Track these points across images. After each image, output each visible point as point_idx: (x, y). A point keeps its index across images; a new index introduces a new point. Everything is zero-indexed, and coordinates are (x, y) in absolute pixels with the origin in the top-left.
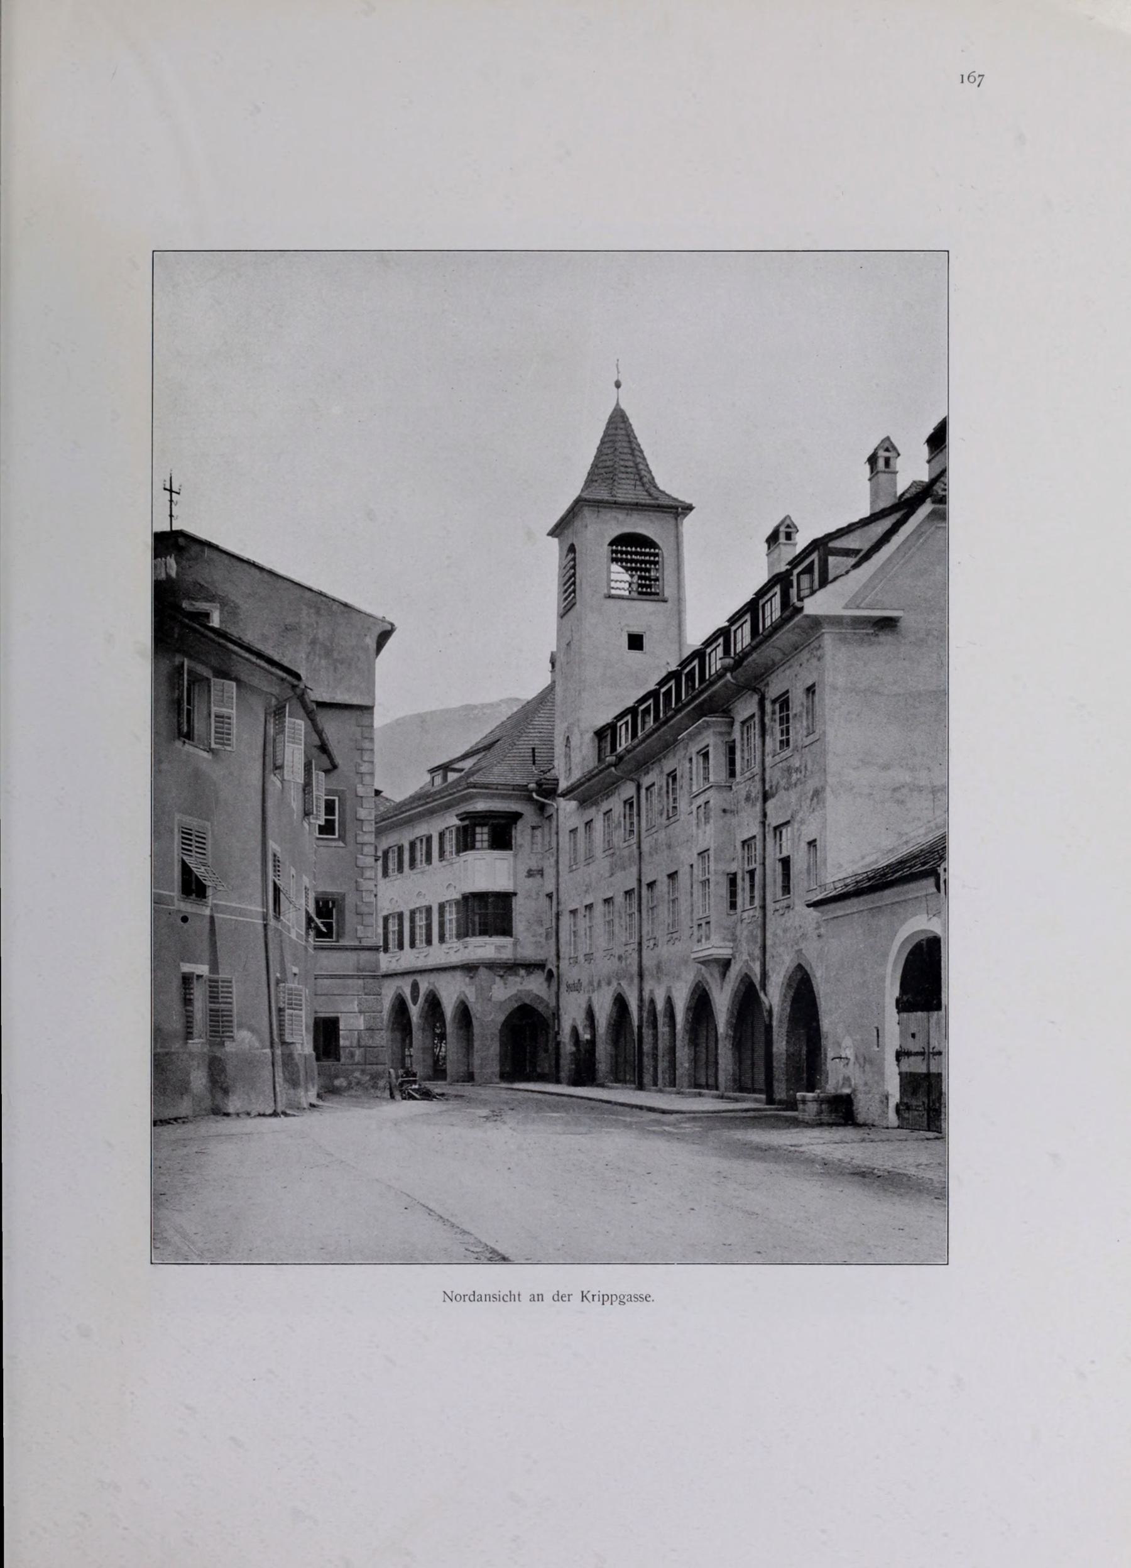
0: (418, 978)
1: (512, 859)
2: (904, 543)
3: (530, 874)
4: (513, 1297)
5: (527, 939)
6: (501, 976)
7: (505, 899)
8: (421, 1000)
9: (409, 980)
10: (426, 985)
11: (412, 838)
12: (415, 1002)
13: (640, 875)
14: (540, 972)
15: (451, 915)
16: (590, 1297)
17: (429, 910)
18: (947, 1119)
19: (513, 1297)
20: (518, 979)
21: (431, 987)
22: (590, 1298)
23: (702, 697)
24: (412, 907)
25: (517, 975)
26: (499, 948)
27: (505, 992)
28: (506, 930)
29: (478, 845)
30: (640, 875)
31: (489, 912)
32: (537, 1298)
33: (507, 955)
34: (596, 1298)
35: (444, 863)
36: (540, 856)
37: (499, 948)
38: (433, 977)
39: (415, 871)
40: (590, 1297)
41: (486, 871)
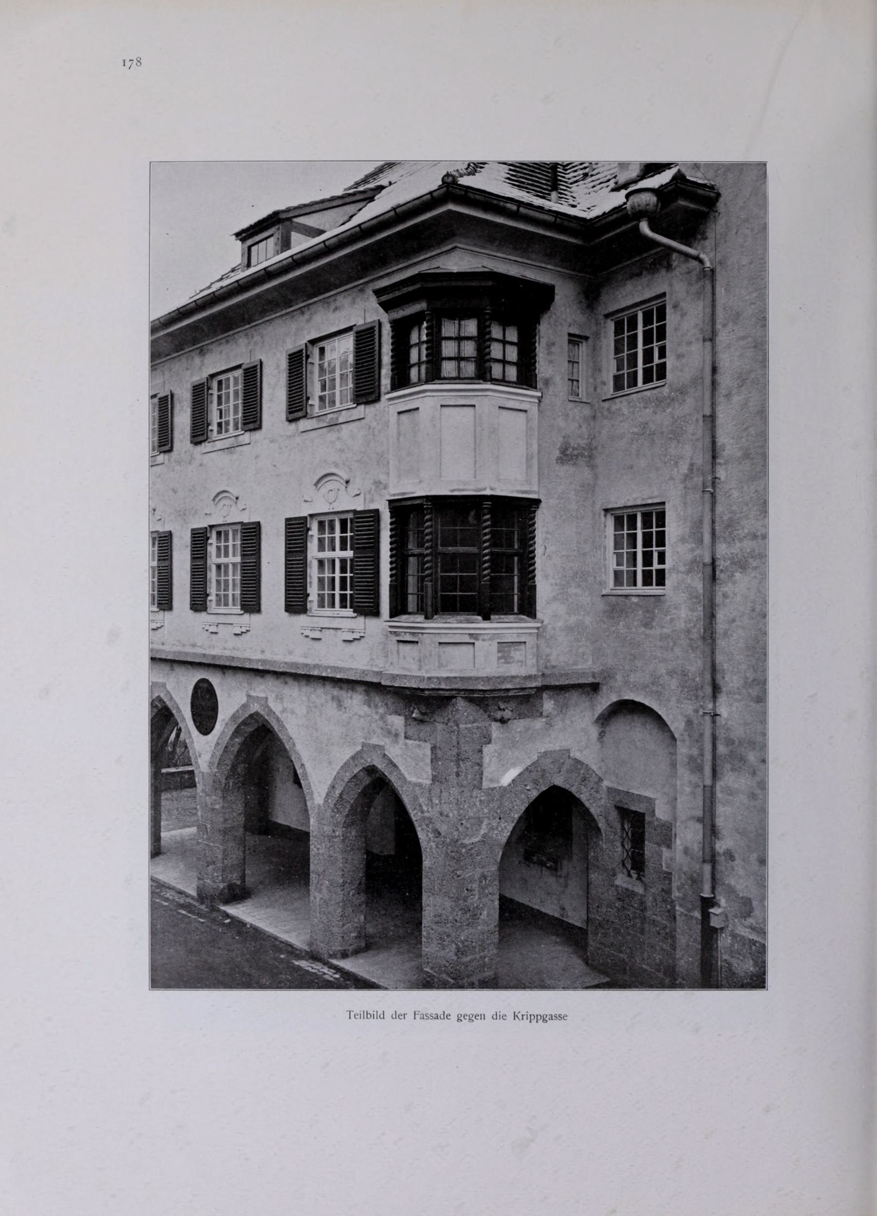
1: (534, 410)
2: (341, 396)
3: (567, 455)
5: (569, 610)
6: (503, 721)
7: (513, 516)
11: (200, 376)
15: (324, 554)
16: (520, 1016)
17: (252, 534)
21: (255, 708)
22: (520, 1017)
24: (201, 523)
26: (505, 648)
27: (510, 763)
29: (448, 368)
31: (465, 555)
33: (522, 667)
34: (525, 1017)
35: (304, 424)
36: (587, 411)
37: (182, 432)
38: (263, 689)
39: (206, 447)
40: (520, 1016)
41: (459, 438)
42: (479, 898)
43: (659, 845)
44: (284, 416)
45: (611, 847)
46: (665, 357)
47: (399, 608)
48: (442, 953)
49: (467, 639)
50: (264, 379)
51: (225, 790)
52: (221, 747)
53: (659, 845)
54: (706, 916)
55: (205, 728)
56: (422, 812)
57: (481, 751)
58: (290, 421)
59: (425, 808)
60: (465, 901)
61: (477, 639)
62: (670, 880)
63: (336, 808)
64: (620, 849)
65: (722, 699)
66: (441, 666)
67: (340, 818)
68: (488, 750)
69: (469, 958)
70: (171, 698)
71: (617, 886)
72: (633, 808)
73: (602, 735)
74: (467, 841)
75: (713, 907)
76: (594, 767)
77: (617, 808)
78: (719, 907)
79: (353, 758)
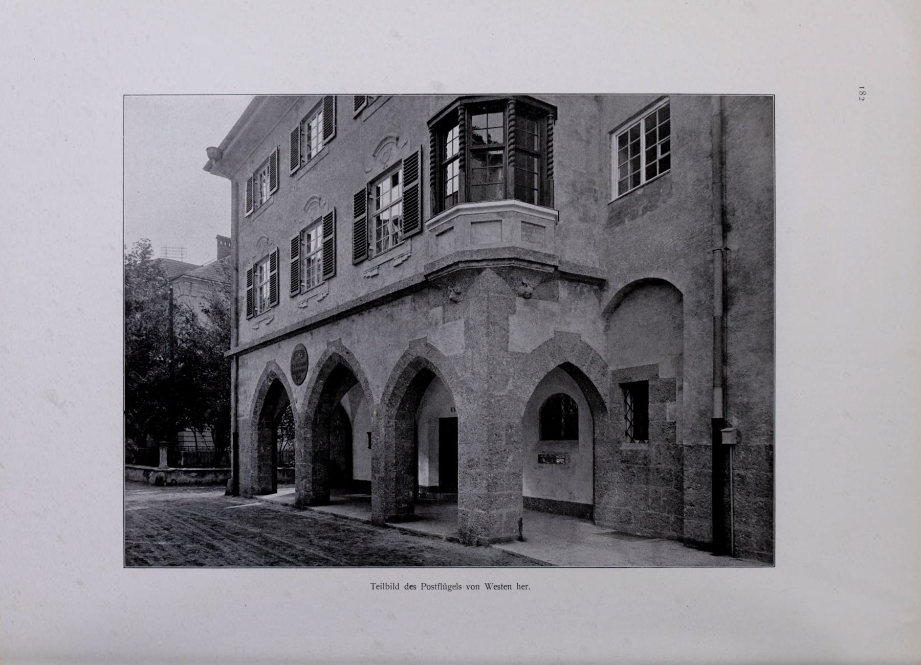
0: (305, 340)
4: (396, 587)
6: (526, 296)
8: (311, 376)
9: (288, 348)
10: (322, 347)
12: (298, 380)
13: (721, 184)
14: (593, 299)
18: (755, 565)
19: (396, 587)
20: (554, 307)
23: (233, 394)
25: (554, 298)
28: (533, 187)
30: (721, 184)
32: (412, 587)
38: (336, 332)
42: (507, 444)
43: (663, 401)
44: (350, 261)
45: (618, 420)
46: (634, 160)
47: (426, 476)
48: (475, 491)
49: (496, 218)
50: (338, 264)
51: (315, 424)
52: (310, 390)
53: (663, 401)
54: (717, 438)
55: (298, 380)
56: (458, 378)
57: (507, 319)
58: (356, 265)
59: (460, 375)
60: (494, 443)
61: (504, 217)
62: (675, 428)
63: (390, 404)
64: (624, 421)
65: (731, 235)
66: (472, 243)
67: (394, 411)
68: (513, 320)
69: (498, 493)
70: (279, 369)
71: (622, 451)
72: (635, 380)
73: (607, 328)
74: (495, 393)
75: (725, 427)
76: (602, 354)
77: (623, 386)
78: (731, 426)
79: (403, 357)
